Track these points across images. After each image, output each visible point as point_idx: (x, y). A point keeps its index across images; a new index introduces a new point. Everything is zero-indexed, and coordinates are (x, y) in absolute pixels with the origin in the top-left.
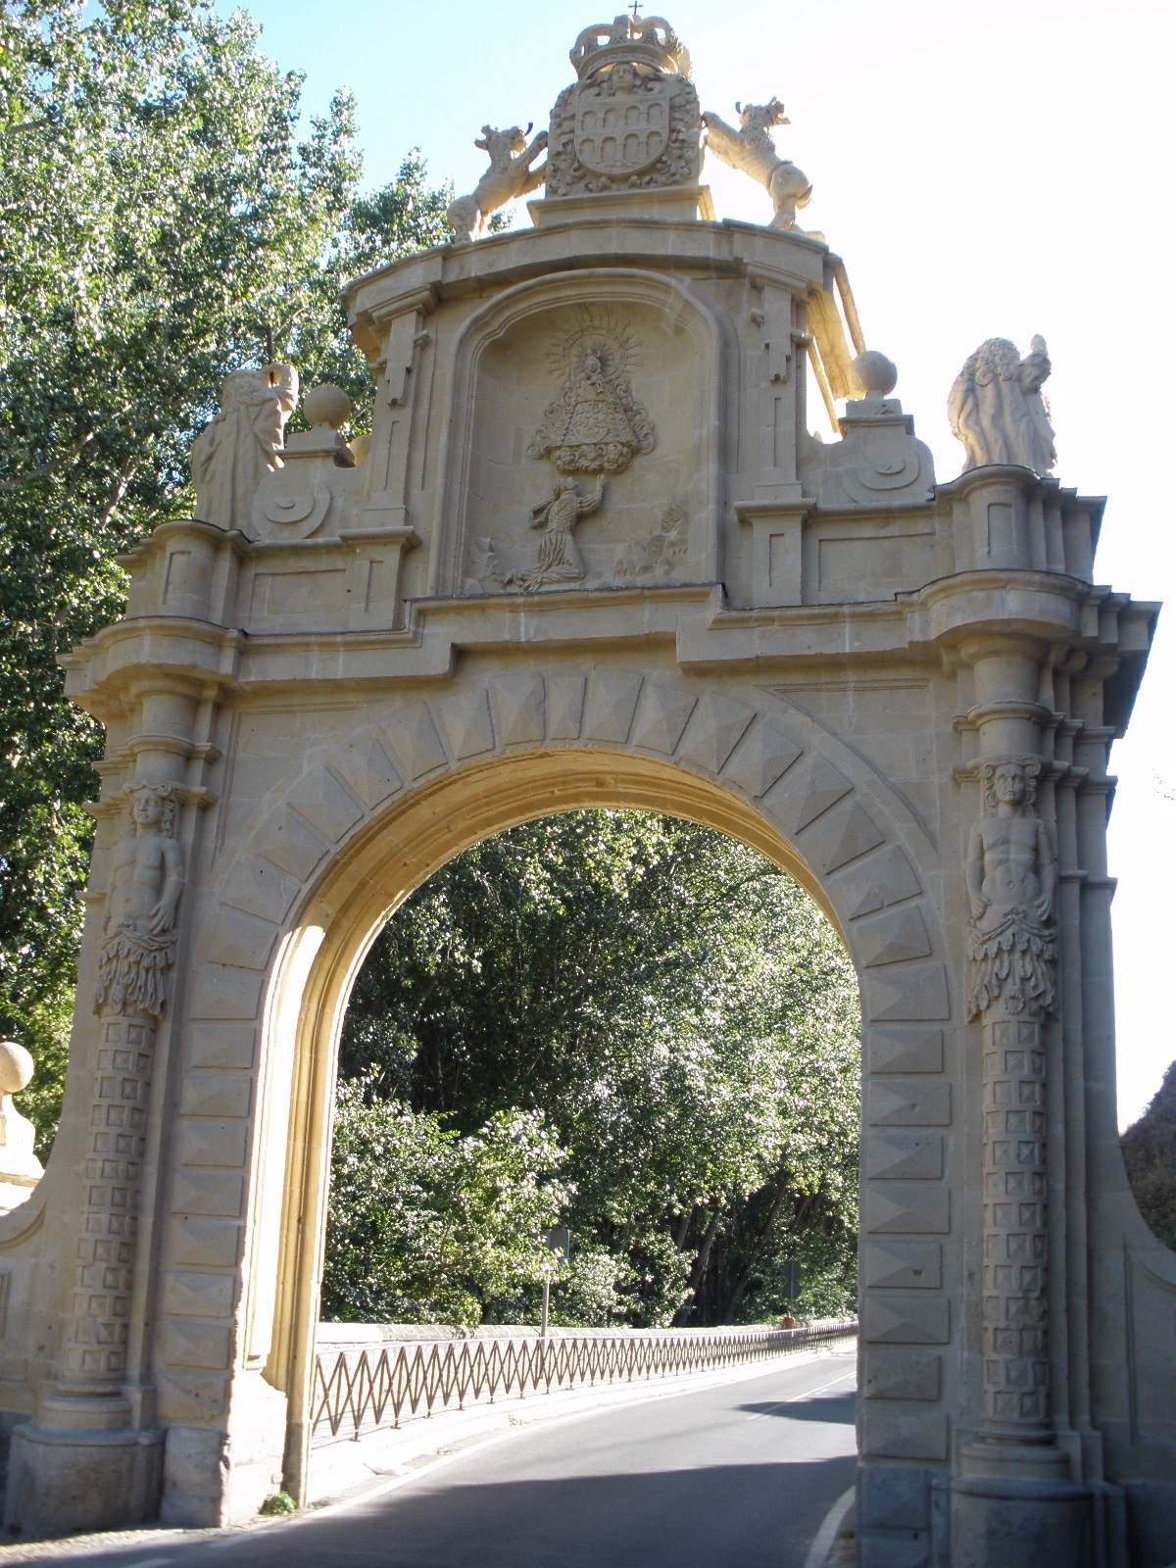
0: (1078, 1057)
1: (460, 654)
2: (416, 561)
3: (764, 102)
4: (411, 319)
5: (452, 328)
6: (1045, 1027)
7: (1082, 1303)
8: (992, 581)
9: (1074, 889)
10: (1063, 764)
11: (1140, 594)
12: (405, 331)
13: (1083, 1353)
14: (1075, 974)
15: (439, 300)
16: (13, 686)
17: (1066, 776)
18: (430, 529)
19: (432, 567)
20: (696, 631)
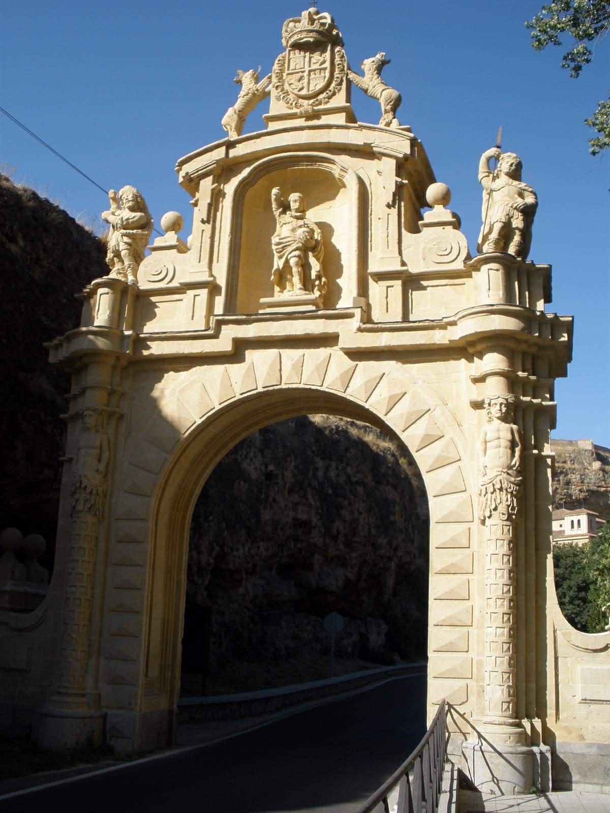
20: (349, 333)
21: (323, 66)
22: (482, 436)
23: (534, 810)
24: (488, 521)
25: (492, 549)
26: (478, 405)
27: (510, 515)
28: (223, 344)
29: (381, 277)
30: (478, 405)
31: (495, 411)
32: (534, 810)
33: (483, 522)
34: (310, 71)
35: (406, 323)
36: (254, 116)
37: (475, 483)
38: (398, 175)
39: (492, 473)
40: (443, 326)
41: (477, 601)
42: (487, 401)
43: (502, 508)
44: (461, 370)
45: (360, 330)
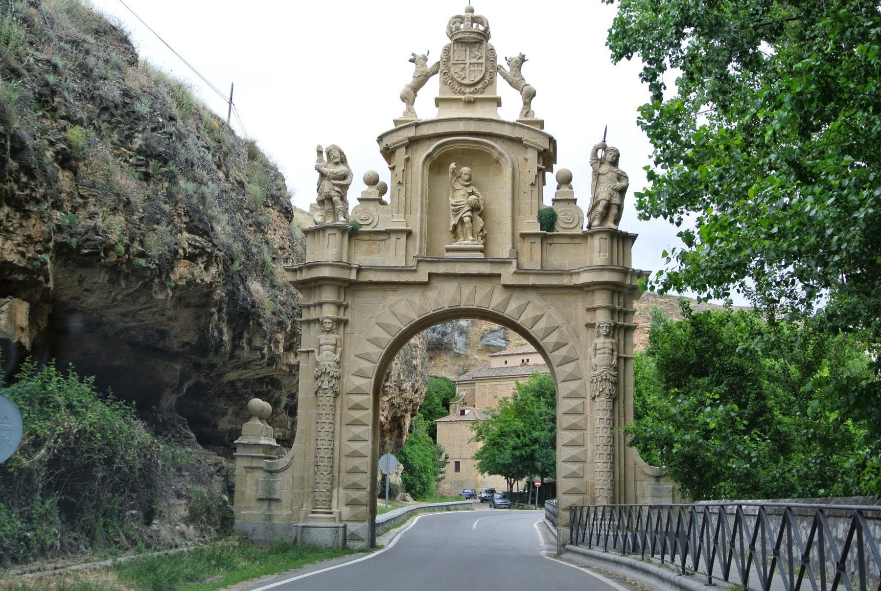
0: (622, 409)
1: (430, 275)
2: (411, 242)
3: (435, 44)
4: (403, 149)
5: (421, 154)
6: (614, 403)
7: (623, 479)
8: (602, 269)
9: (622, 361)
10: (621, 323)
11: (644, 268)
12: (401, 155)
13: (615, 256)
14: (622, 385)
15: (413, 143)
16: (829, 5)
17: (622, 326)
18: (416, 230)
19: (418, 243)
20: (508, 276)
21: (480, 61)
22: (593, 346)
23: (339, 467)
24: (597, 399)
25: (601, 415)
26: (590, 326)
27: (611, 395)
28: (422, 276)
29: (524, 236)
30: (590, 326)
31: (603, 331)
32: (339, 467)
33: (594, 398)
34: (470, 64)
35: (543, 272)
36: (74, 376)
37: (588, 374)
38: (539, 163)
39: (599, 370)
40: (570, 274)
41: (590, 446)
42: (597, 324)
43: (607, 391)
44: (578, 306)
45: (515, 273)
